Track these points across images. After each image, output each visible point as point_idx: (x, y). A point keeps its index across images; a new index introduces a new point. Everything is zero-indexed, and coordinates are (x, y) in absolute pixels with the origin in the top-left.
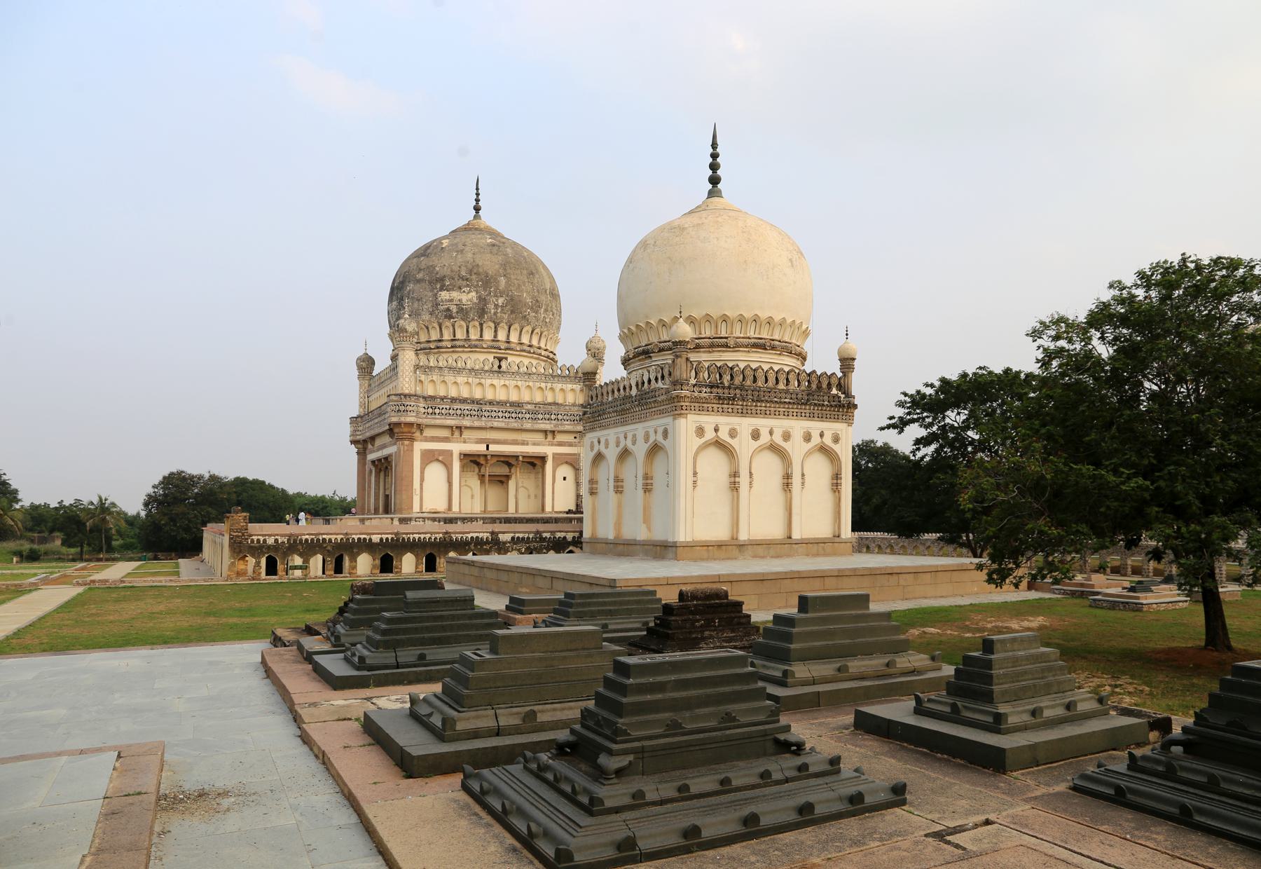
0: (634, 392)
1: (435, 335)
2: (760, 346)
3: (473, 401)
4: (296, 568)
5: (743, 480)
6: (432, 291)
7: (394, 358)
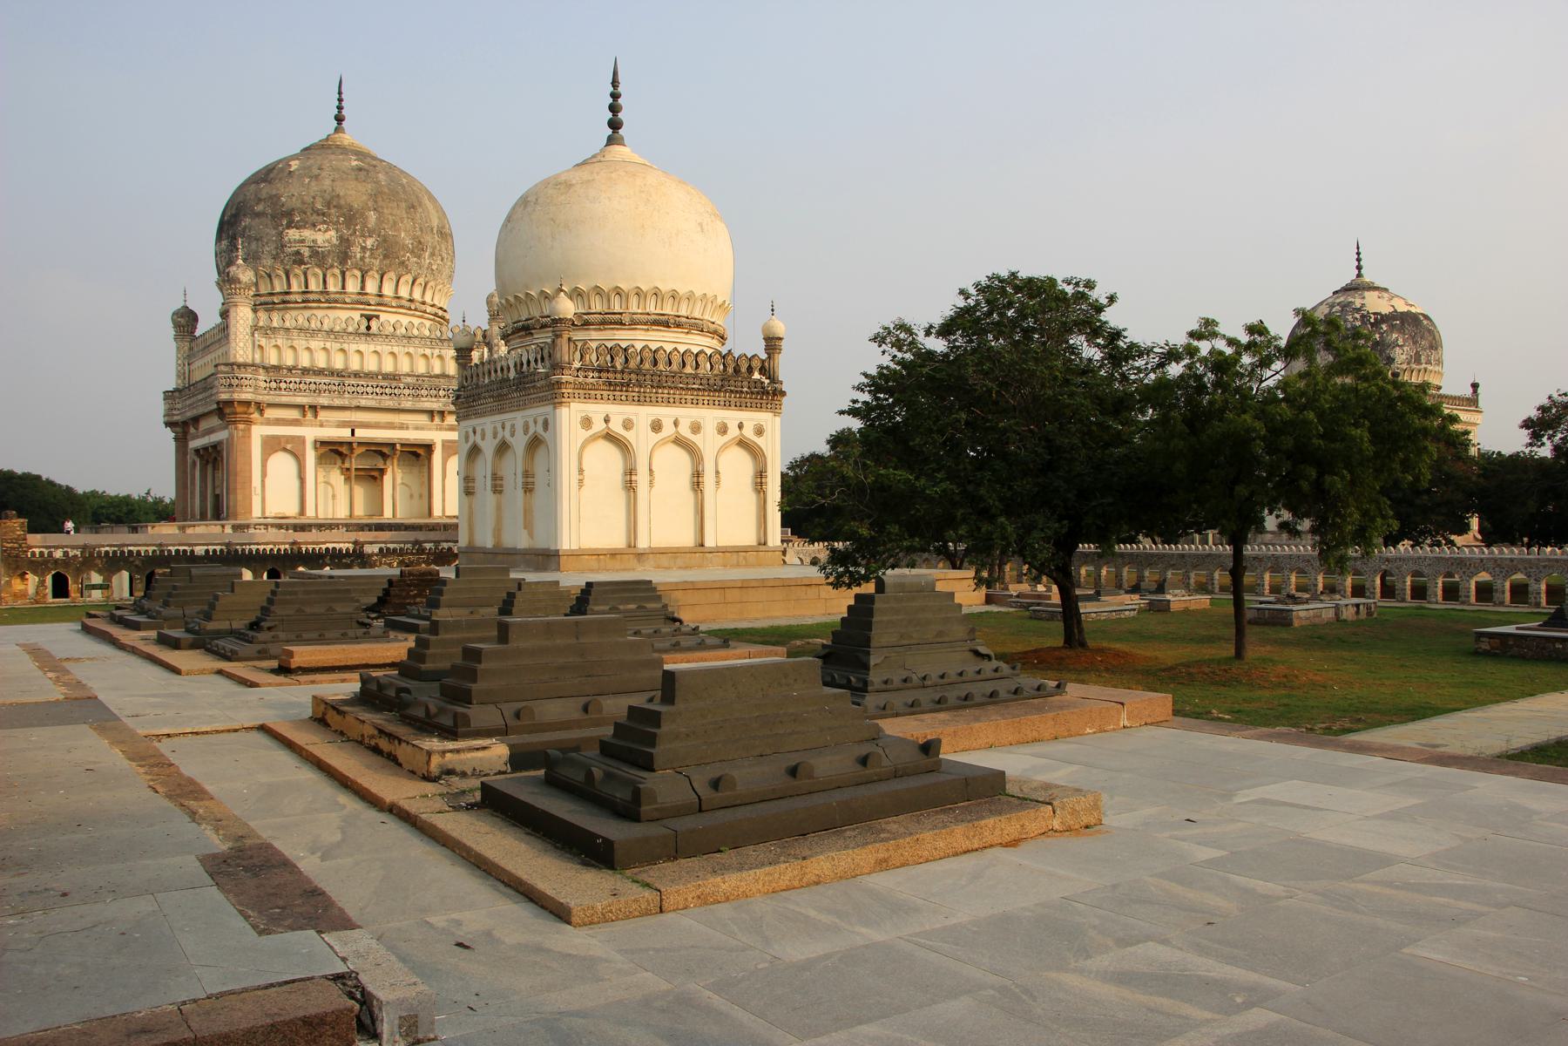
0: (512, 374)
2: (663, 323)
3: (333, 373)
4: (94, 587)
5: (642, 478)
7: (225, 314)
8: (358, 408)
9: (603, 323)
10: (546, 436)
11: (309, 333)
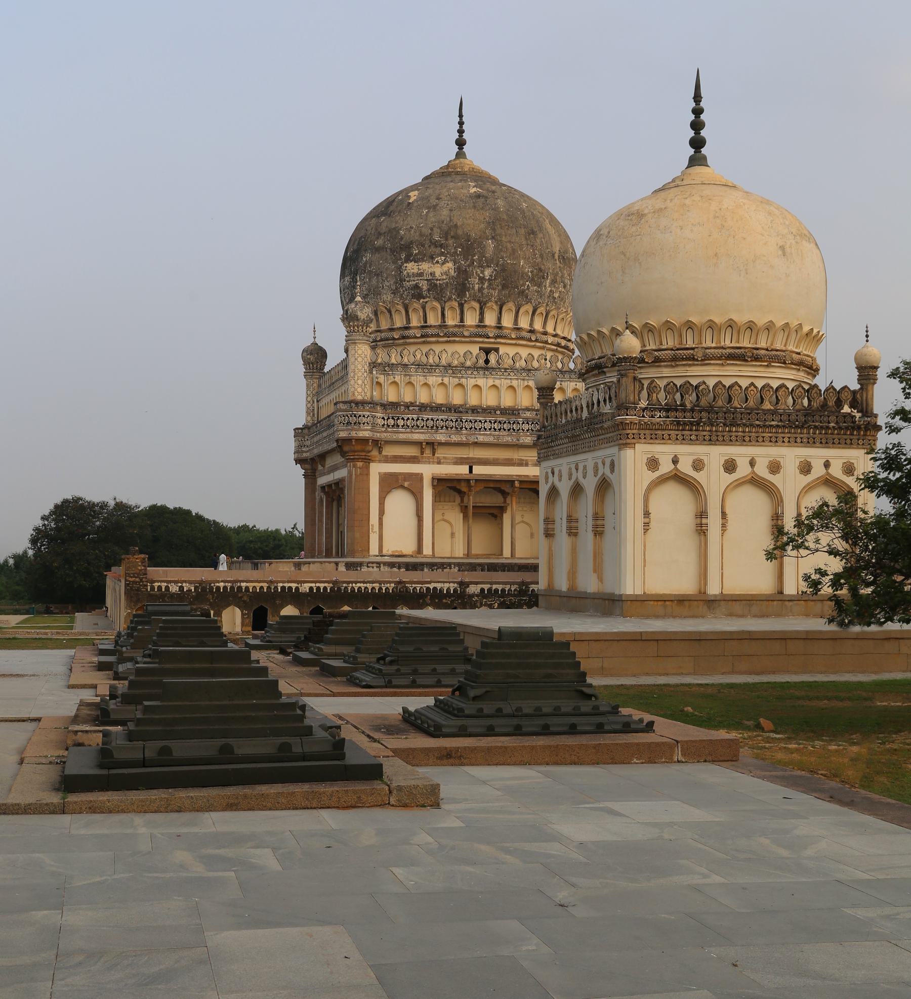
0: (585, 414)
1: (399, 322)
2: (739, 356)
5: (713, 522)
6: (394, 262)
8: (476, 444)
9: (675, 359)
10: (612, 477)
11: (427, 368)
